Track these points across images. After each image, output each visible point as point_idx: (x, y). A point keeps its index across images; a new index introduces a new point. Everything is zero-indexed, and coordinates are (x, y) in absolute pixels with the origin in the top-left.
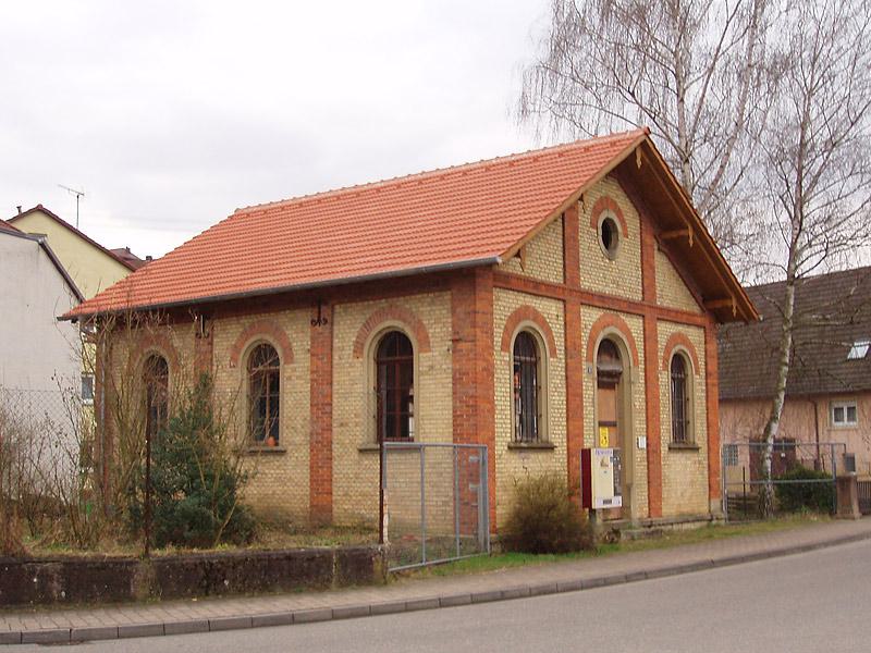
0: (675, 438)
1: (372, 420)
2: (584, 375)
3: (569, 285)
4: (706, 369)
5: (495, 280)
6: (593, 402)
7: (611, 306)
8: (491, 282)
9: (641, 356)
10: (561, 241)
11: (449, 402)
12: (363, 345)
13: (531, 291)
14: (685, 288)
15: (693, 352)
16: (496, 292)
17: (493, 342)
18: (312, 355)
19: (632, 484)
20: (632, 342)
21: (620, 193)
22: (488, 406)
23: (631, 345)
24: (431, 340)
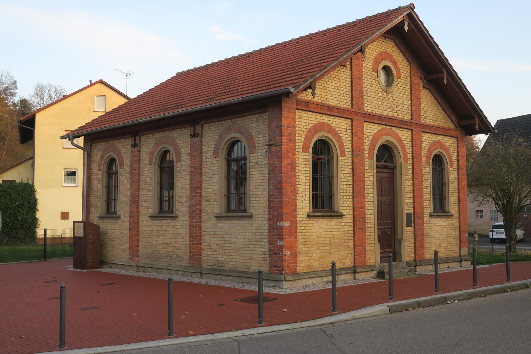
0: (435, 208)
1: (224, 198)
2: (366, 168)
3: (355, 109)
4: (458, 164)
5: (297, 105)
6: (373, 186)
7: (387, 123)
8: (294, 106)
9: (409, 156)
10: (349, 80)
11: (266, 185)
12: (218, 150)
13: (326, 113)
14: (443, 112)
15: (448, 153)
16: (298, 113)
17: (295, 146)
18: (191, 157)
19: (402, 239)
20: (403, 147)
21: (396, 49)
22: (292, 189)
23: (402, 149)
24: (257, 145)
